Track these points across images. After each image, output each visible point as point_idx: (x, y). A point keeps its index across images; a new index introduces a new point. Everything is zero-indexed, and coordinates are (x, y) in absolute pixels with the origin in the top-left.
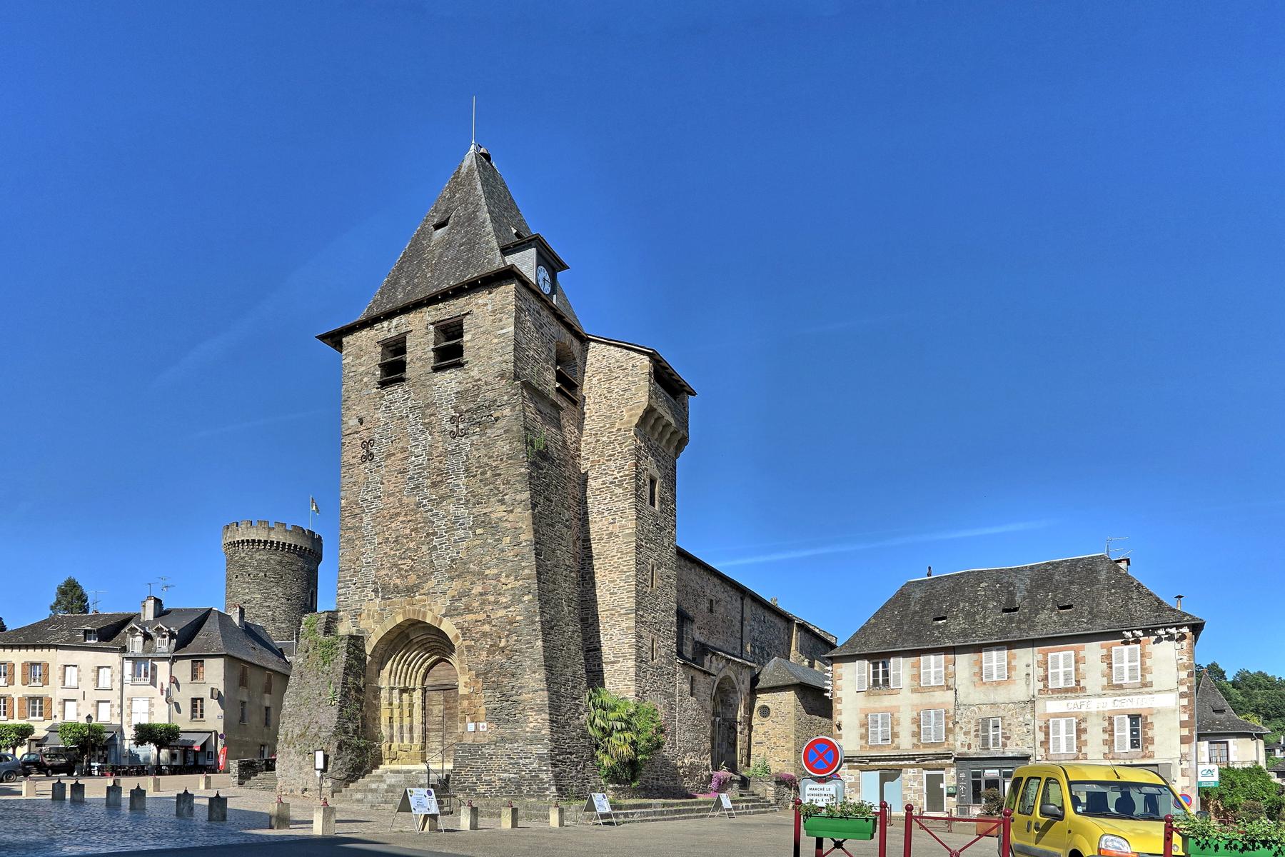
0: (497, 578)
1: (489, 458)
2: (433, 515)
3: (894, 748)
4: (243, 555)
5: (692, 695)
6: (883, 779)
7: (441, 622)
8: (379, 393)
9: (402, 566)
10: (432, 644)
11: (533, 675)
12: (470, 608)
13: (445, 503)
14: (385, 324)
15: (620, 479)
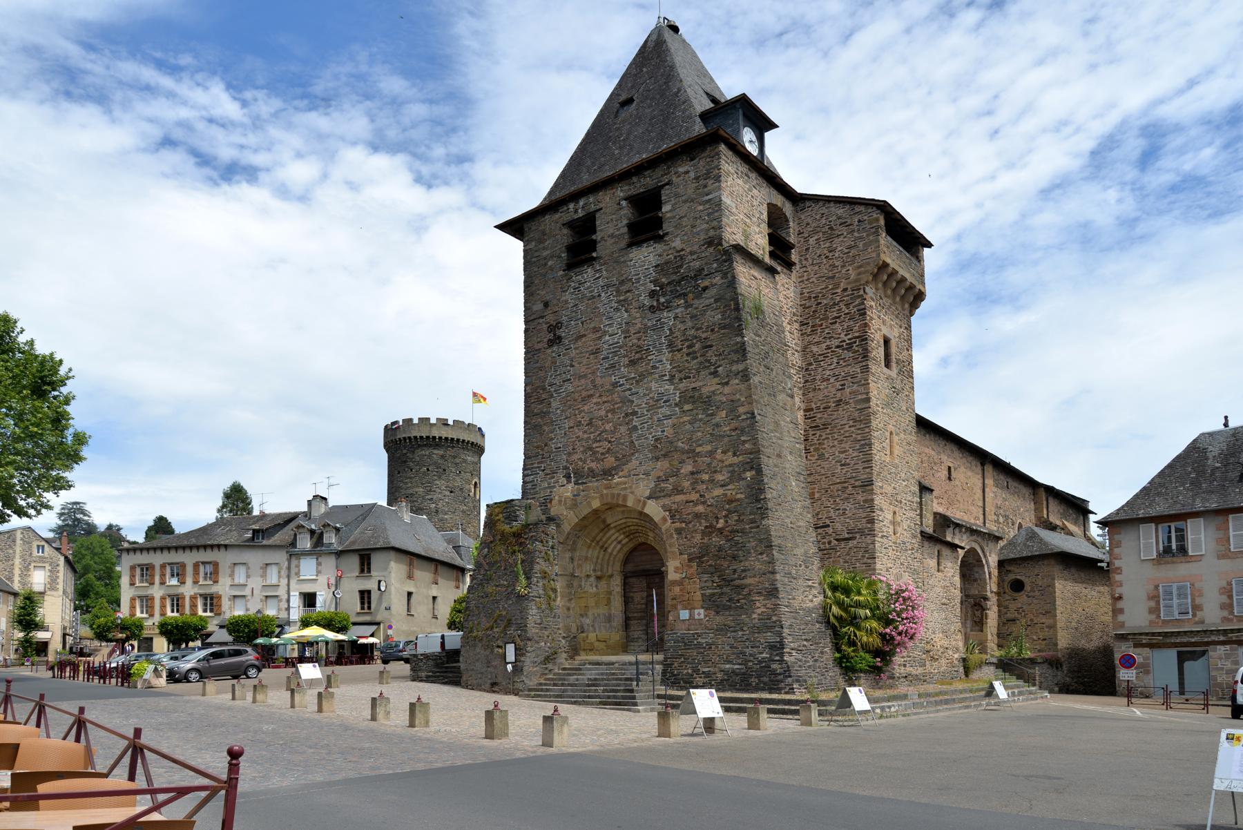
0: (711, 454)
1: (697, 329)
2: (633, 394)
3: (1196, 623)
4: (405, 451)
5: (938, 571)
6: (1182, 658)
7: (645, 504)
8: (566, 275)
9: (598, 449)
10: (632, 528)
11: (760, 557)
12: (680, 489)
13: (645, 380)
14: (571, 206)
15: (848, 342)
